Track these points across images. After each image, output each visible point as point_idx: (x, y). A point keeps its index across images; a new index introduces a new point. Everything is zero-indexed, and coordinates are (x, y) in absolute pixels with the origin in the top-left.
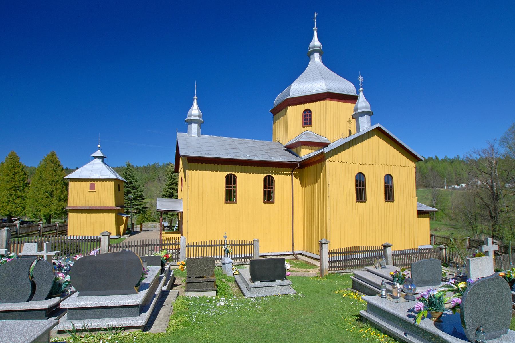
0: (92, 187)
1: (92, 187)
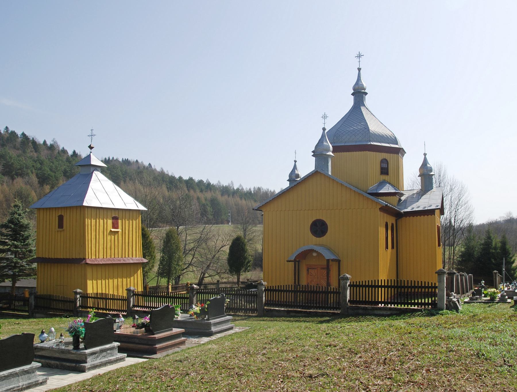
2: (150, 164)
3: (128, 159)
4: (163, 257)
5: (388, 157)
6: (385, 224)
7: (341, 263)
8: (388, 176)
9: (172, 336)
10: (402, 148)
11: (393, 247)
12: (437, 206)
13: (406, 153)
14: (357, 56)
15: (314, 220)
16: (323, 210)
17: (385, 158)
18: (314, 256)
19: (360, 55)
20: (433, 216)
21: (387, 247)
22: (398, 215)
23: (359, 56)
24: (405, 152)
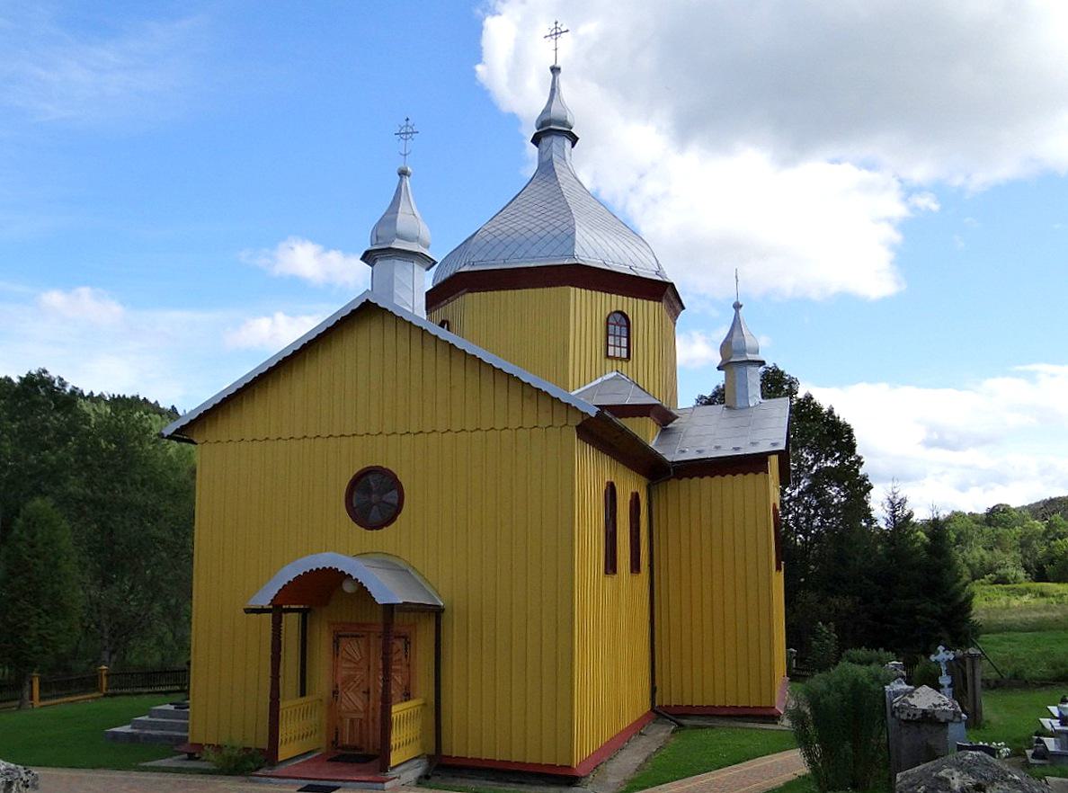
2: (156, 402)
3: (124, 396)
4: (1039, 533)
5: (630, 310)
6: (603, 487)
7: (445, 617)
8: (616, 576)
9: (62, 767)
10: (672, 284)
11: (635, 567)
12: (774, 445)
13: (683, 308)
14: (551, 35)
15: (358, 470)
16: (387, 435)
17: (620, 309)
18: (343, 591)
19: (558, 31)
20: (762, 474)
21: (611, 566)
22: (656, 471)
23: (556, 34)
24: (680, 301)
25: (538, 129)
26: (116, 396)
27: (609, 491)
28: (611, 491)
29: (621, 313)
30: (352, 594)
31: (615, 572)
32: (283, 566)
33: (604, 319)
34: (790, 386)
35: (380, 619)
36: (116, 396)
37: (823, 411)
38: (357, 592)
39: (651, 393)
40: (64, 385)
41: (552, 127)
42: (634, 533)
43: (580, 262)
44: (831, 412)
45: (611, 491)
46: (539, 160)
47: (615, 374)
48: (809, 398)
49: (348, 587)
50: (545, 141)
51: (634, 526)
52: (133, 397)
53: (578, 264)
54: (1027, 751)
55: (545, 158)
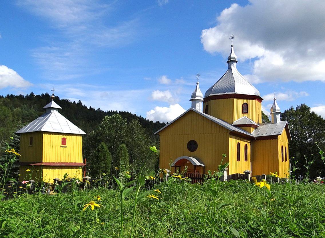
0: (64, 141)
1: (64, 141)
11: (246, 159)
17: (246, 102)
21: (239, 159)
25: (228, 60)
26: (113, 111)
27: (238, 145)
28: (239, 145)
29: (246, 103)
30: (188, 164)
31: (247, 160)
32: (176, 158)
33: (242, 105)
34: (308, 109)
35: (193, 168)
36: (113, 111)
37: (318, 117)
38: (189, 163)
39: (253, 120)
40: (66, 99)
41: (231, 60)
42: (246, 152)
43: (236, 93)
44: (320, 116)
45: (239, 145)
46: (229, 67)
47: (244, 117)
48: (313, 113)
49: (188, 162)
50: (230, 63)
51: (246, 151)
52: (125, 112)
53: (235, 94)
54: (28, 104)
55: (230, 67)
